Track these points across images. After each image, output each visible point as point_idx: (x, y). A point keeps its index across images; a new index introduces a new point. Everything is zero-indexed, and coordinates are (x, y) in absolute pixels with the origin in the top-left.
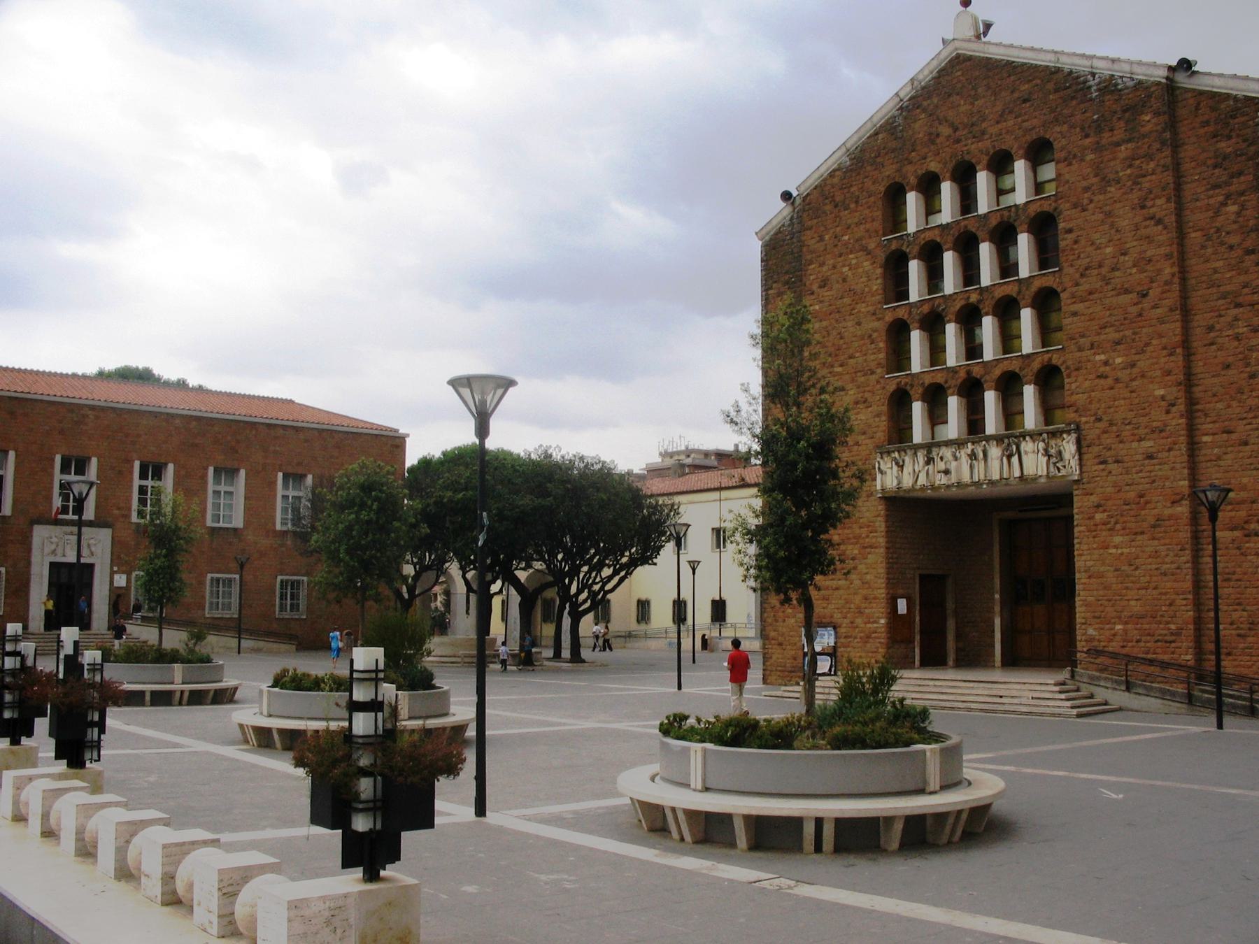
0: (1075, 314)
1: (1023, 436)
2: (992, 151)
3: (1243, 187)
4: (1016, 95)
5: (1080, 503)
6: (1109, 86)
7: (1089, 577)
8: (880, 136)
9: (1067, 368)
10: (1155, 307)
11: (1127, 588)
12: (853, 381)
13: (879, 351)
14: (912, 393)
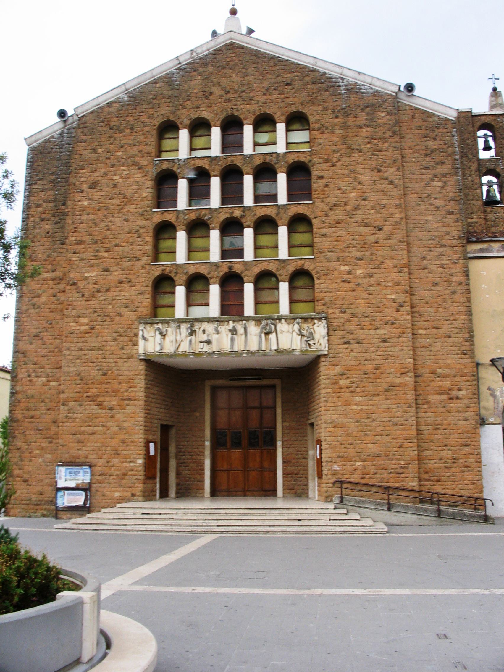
0: (324, 235)
1: (280, 319)
2: (258, 113)
3: (445, 172)
4: (280, 79)
5: (324, 370)
6: (354, 89)
7: (335, 427)
8: (158, 85)
9: (317, 273)
10: (388, 238)
11: (366, 435)
12: (117, 264)
13: (146, 243)
14: (175, 279)
